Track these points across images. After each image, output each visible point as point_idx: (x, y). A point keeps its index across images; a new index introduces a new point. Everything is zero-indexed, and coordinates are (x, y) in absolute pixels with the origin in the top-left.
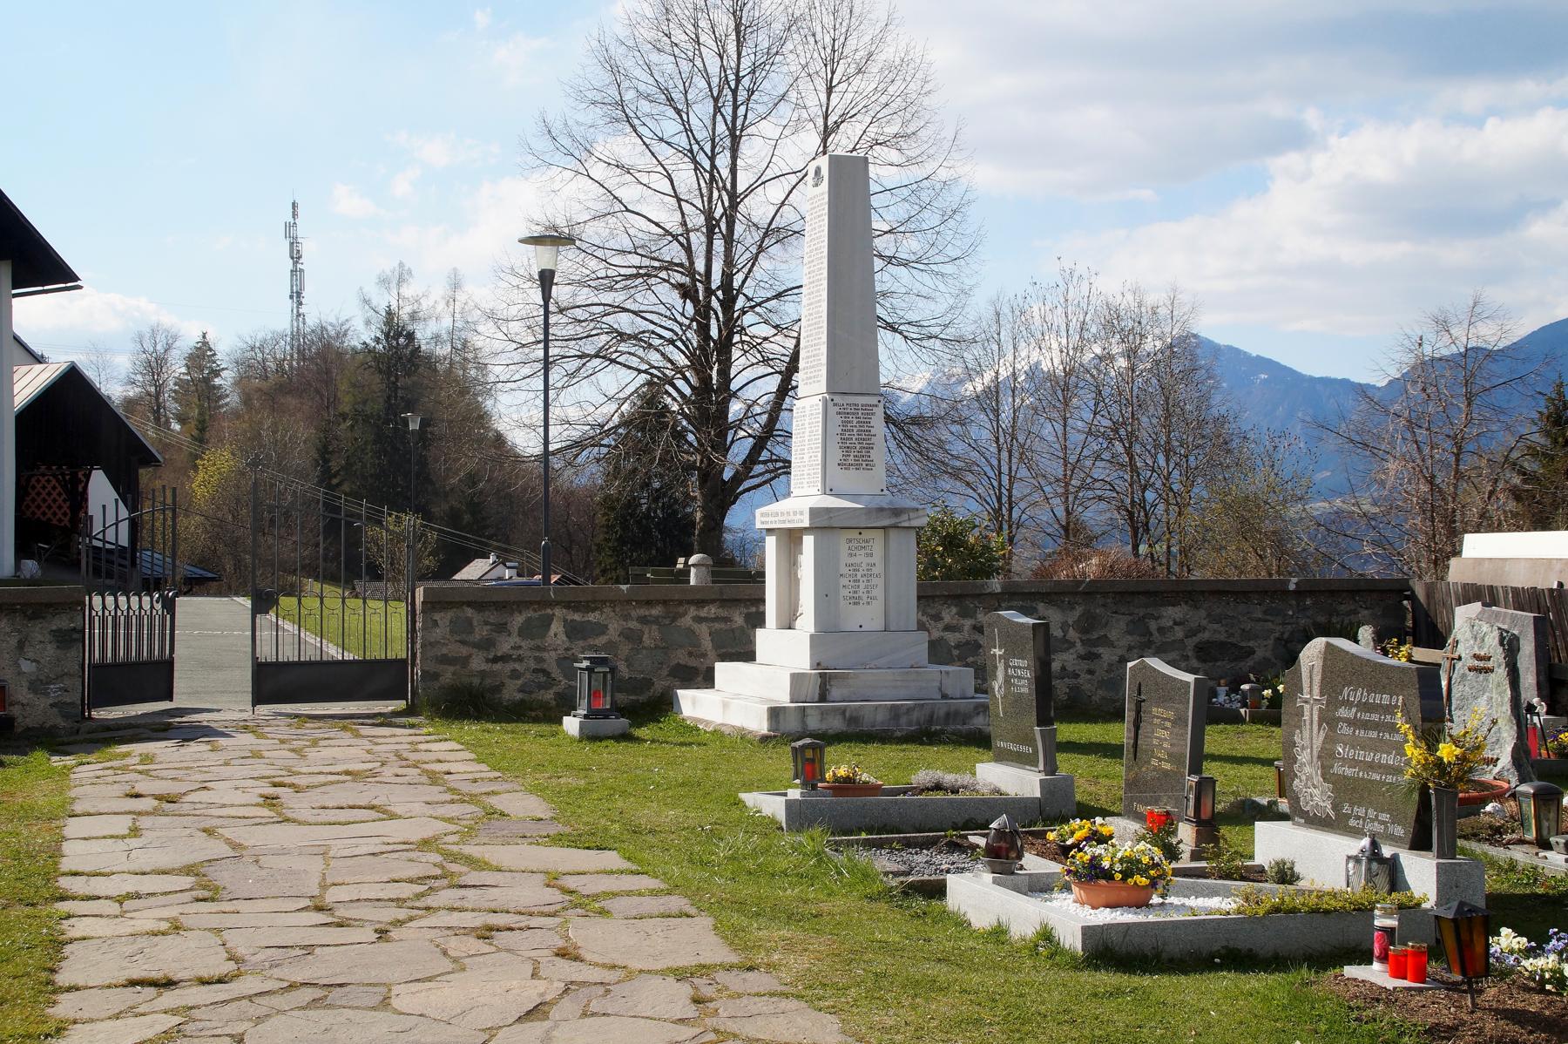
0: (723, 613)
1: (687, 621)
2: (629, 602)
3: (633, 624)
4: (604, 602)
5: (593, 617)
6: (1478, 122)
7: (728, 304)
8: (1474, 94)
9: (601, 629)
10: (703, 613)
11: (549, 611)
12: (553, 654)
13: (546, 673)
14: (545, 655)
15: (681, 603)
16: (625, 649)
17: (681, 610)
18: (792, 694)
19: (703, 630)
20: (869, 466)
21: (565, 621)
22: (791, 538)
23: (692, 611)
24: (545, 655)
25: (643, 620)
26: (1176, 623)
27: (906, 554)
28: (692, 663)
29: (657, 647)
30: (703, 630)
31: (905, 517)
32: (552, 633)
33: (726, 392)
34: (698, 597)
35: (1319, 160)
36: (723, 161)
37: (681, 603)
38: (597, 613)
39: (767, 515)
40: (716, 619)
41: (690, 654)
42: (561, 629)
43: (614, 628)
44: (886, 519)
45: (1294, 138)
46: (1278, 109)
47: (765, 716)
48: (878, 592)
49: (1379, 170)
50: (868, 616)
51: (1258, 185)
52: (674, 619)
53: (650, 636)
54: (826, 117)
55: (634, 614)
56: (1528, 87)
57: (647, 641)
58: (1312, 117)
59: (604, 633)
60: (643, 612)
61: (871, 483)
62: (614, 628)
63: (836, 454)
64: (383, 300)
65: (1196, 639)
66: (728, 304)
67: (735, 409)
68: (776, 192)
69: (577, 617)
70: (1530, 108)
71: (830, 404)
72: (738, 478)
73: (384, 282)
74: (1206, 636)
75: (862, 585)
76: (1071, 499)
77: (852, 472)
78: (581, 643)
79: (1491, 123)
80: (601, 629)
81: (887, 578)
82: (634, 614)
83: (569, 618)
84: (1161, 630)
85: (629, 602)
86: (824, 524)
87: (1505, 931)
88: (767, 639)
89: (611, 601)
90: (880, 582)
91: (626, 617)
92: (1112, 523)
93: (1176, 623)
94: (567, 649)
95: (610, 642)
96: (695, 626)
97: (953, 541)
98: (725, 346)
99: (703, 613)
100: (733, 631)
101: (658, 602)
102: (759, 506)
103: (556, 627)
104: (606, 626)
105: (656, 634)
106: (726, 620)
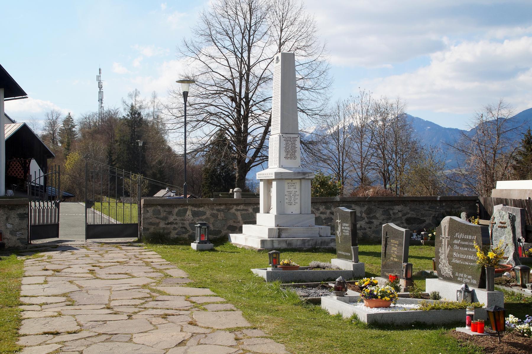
0: (245, 208)
1: (233, 211)
2: (213, 204)
3: (215, 212)
4: (205, 204)
5: (201, 209)
6: (501, 41)
7: (247, 103)
8: (500, 32)
9: (204, 213)
10: (239, 208)
11: (186, 207)
12: (188, 222)
13: (185, 228)
14: (185, 222)
15: (231, 204)
16: (212, 220)
17: (231, 207)
18: (269, 235)
19: (239, 214)
20: (295, 158)
21: (192, 210)
22: (268, 183)
23: (235, 207)
24: (185, 222)
25: (218, 210)
26: (399, 211)
27: (308, 188)
28: (235, 225)
29: (223, 219)
30: (239, 214)
31: (307, 175)
32: (187, 215)
33: (246, 133)
34: (237, 202)
35: (448, 54)
36: (245, 55)
37: (231, 204)
38: (203, 208)
39: (260, 174)
40: (243, 210)
41: (234, 222)
42: (190, 213)
43: (208, 213)
44: (301, 176)
45: (439, 47)
46: (434, 37)
47: (260, 243)
48: (298, 201)
49: (468, 58)
50: (295, 209)
51: (427, 63)
52: (229, 210)
53: (221, 216)
55: (215, 208)
56: (518, 30)
57: (219, 217)
58: (445, 40)
59: (205, 215)
60: (218, 207)
61: (296, 164)
62: (208, 213)
63: (284, 154)
64: (130, 102)
65: (406, 217)
66: (247, 103)
67: (250, 139)
68: (263, 65)
69: (196, 209)
70: (519, 37)
71: (282, 137)
72: (250, 162)
73: (130, 95)
74: (409, 216)
75: (292, 198)
76: (363, 169)
77: (289, 160)
78: (197, 218)
79: (506, 42)
80: (204, 213)
81: (301, 196)
82: (215, 208)
83: (193, 209)
84: (394, 214)
85: (213, 204)
86: (280, 178)
87: (511, 316)
88: (260, 217)
89: (207, 204)
90: (299, 197)
91: (213, 209)
92: (377, 177)
93: (399, 211)
94: (192, 220)
95: (207, 218)
96: (236, 212)
97: (323, 183)
98: (246, 117)
99: (239, 208)
100: (249, 214)
101: (223, 204)
102: (258, 172)
103: (189, 213)
104: (206, 212)
105: (223, 215)
106: (246, 210)
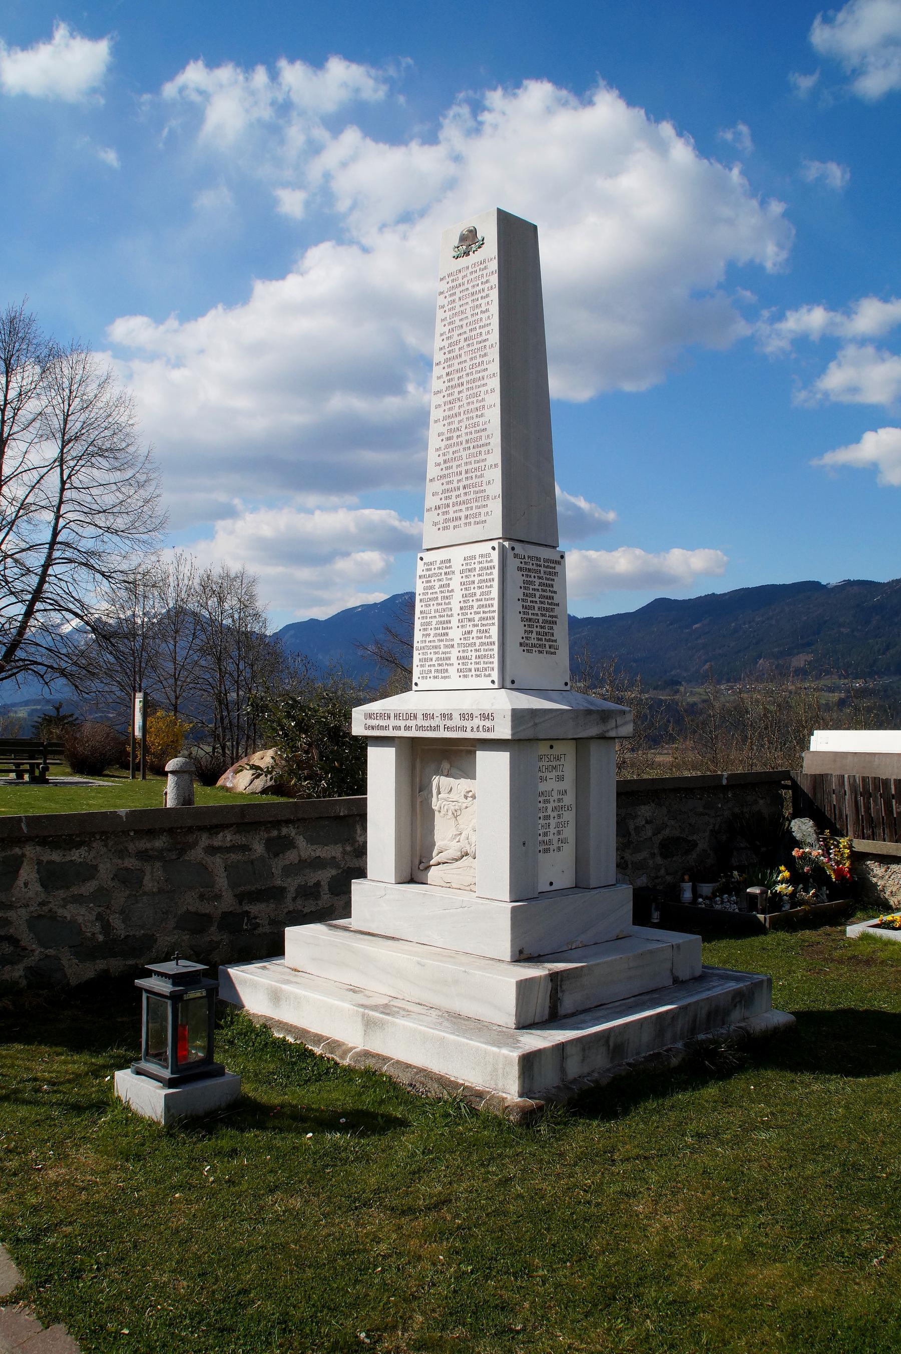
0: (240, 839)
1: (197, 854)
2: (125, 833)
3: (130, 863)
4: (93, 834)
5: (77, 855)
6: (311, 512)
8: (312, 499)
9: (88, 871)
10: (218, 841)
11: (17, 851)
12: (22, 912)
13: (13, 940)
14: (12, 915)
15: (190, 830)
16: (120, 898)
17: (190, 839)
18: (518, 1015)
19: (217, 863)
20: (552, 650)
21: (39, 863)
23: (204, 840)
24: (12, 915)
25: (144, 856)
26: (647, 822)
28: (205, 908)
29: (161, 891)
30: (217, 863)
31: (612, 724)
32: (20, 882)
34: (215, 821)
35: (240, 524)
37: (190, 830)
38: (83, 851)
39: (370, 716)
40: (233, 848)
41: (202, 897)
42: (34, 876)
43: (106, 869)
45: (229, 512)
46: (222, 497)
47: (515, 1071)
48: (569, 832)
49: (267, 531)
51: (210, 535)
52: (182, 851)
53: (153, 877)
54: (64, 435)
55: (131, 847)
56: (334, 499)
57: (149, 884)
58: (237, 501)
59: (92, 877)
60: (143, 844)
62: (106, 869)
63: (517, 630)
65: (660, 837)
69: (56, 856)
70: (335, 509)
71: (510, 554)
74: (667, 832)
75: (553, 822)
76: (178, 689)
77: (535, 655)
78: (62, 893)
79: (318, 513)
80: (88, 871)
82: (131, 847)
83: (45, 858)
84: (637, 829)
85: (125, 833)
89: (103, 833)
90: (569, 816)
91: (122, 853)
93: (647, 822)
94: (42, 904)
95: (100, 889)
96: (209, 860)
99: (218, 841)
100: (252, 862)
101: (162, 831)
102: (360, 702)
103: (28, 873)
104: (95, 868)
105: (160, 874)
106: (245, 848)
